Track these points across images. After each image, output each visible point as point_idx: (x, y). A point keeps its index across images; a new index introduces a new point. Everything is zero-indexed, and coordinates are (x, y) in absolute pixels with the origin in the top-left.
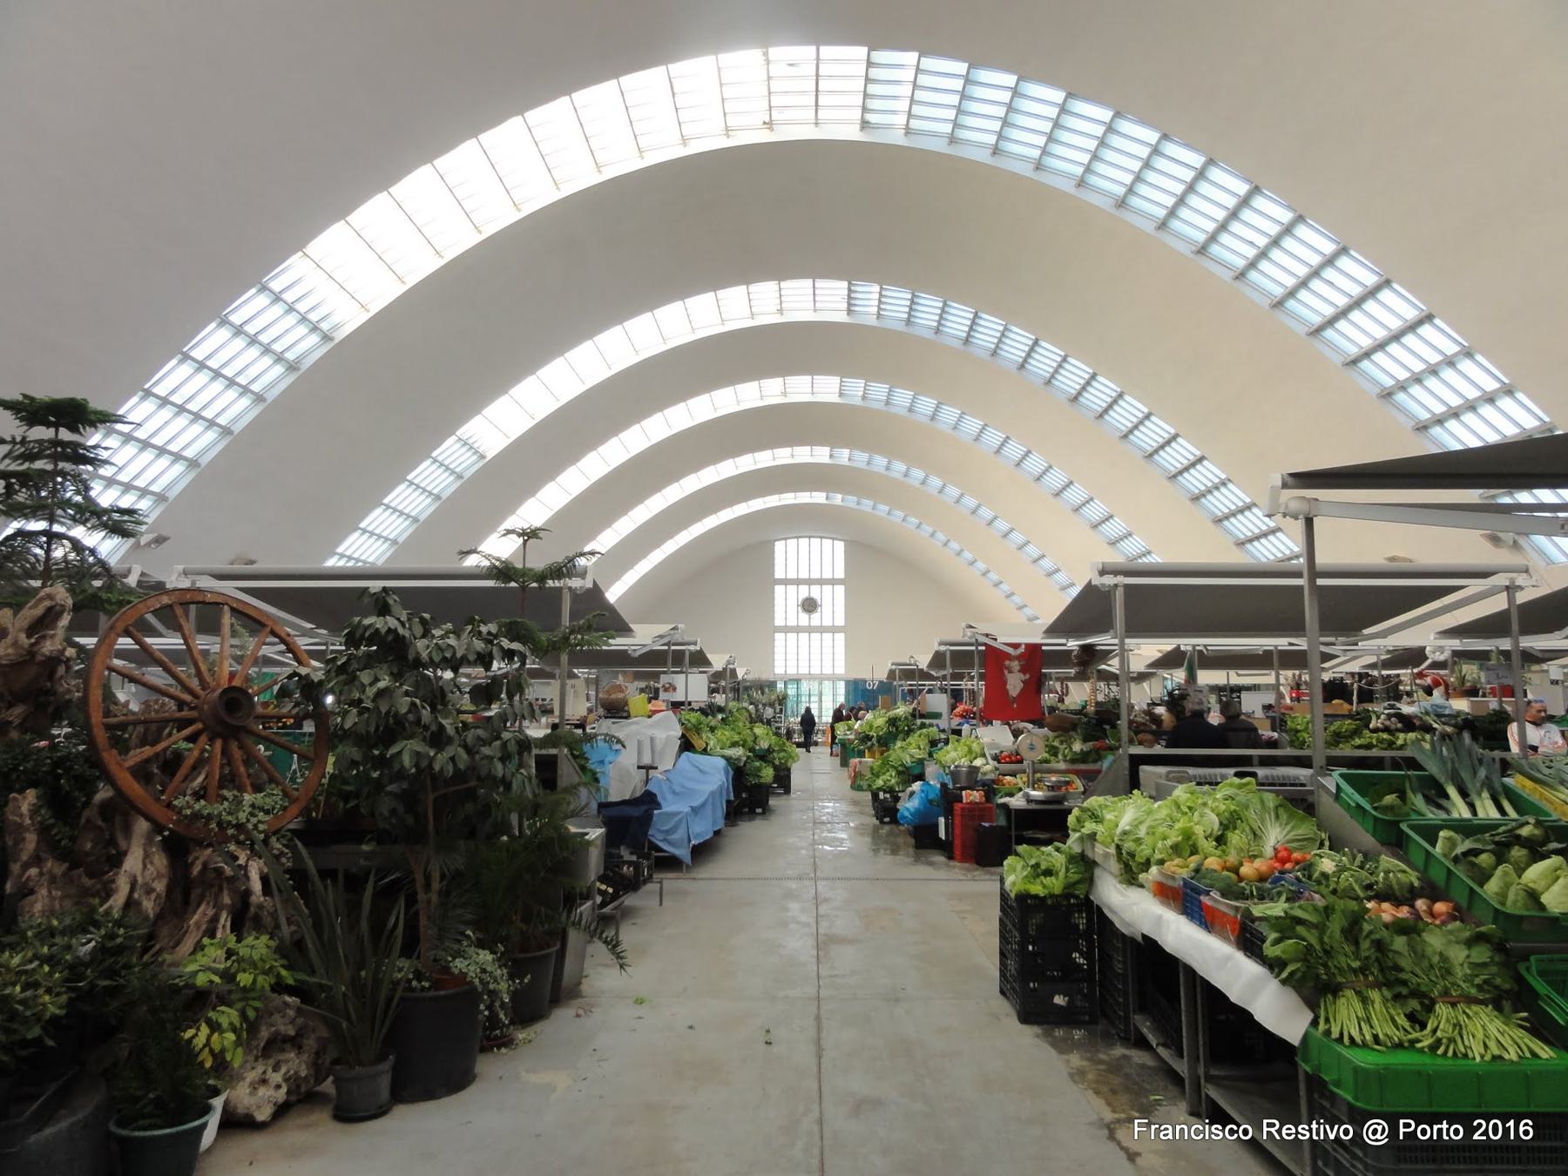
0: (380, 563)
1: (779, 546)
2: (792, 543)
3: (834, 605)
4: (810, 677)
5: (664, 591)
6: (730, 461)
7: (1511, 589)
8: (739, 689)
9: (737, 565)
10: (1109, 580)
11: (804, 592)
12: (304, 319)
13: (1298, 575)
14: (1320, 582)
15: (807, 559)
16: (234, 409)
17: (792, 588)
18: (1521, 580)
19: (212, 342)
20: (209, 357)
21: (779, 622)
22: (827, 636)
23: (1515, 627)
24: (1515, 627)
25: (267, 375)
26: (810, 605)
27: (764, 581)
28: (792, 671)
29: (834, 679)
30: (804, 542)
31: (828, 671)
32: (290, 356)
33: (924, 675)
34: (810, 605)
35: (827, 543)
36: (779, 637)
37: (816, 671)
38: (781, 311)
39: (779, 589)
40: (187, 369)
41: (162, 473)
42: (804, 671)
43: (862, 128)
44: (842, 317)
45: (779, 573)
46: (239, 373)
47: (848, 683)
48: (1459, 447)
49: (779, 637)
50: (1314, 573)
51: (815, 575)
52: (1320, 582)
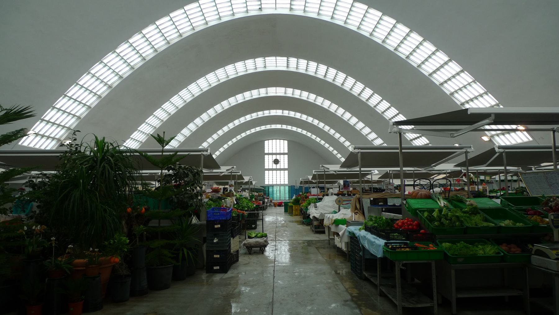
0: (137, 148)
1: (266, 142)
2: (270, 141)
3: (284, 162)
4: (277, 185)
5: (229, 157)
6: (275, 111)
7: (466, 153)
8: (257, 190)
9: (252, 149)
10: (357, 151)
11: (274, 157)
12: (102, 81)
13: (397, 149)
14: (403, 151)
15: (276, 147)
16: (92, 101)
17: (270, 156)
18: (469, 150)
19: (85, 79)
20: (73, 95)
21: (266, 167)
22: (282, 172)
23: (467, 164)
24: (467, 164)
25: (102, 90)
26: (276, 162)
27: (262, 154)
28: (271, 183)
29: (284, 185)
30: (274, 141)
31: (282, 183)
32: (109, 83)
33: (311, 183)
34: (276, 162)
35: (282, 141)
36: (266, 172)
37: (278, 183)
38: (265, 67)
39: (266, 156)
40: (44, 124)
41: (69, 121)
42: (275, 183)
43: (290, 10)
44: (285, 69)
45: (266, 151)
46: (93, 89)
47: (289, 187)
48: (484, 107)
49: (266, 172)
50: (402, 148)
51: (278, 152)
52: (403, 151)
